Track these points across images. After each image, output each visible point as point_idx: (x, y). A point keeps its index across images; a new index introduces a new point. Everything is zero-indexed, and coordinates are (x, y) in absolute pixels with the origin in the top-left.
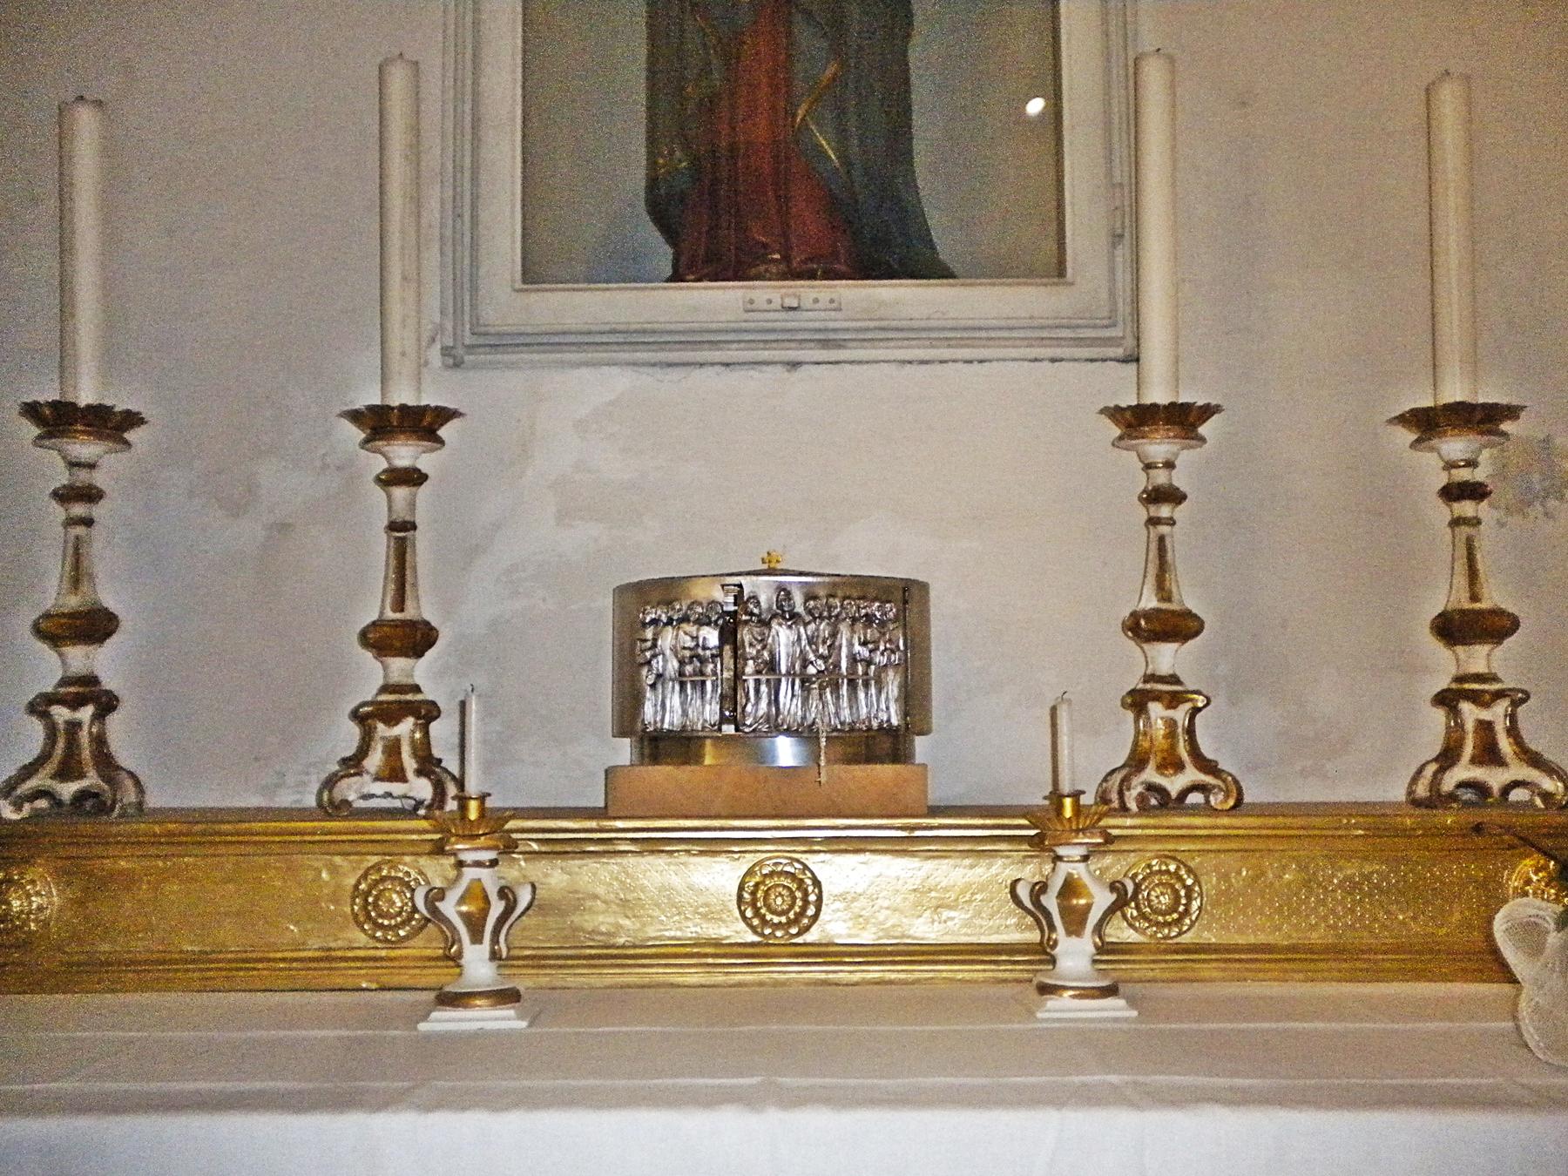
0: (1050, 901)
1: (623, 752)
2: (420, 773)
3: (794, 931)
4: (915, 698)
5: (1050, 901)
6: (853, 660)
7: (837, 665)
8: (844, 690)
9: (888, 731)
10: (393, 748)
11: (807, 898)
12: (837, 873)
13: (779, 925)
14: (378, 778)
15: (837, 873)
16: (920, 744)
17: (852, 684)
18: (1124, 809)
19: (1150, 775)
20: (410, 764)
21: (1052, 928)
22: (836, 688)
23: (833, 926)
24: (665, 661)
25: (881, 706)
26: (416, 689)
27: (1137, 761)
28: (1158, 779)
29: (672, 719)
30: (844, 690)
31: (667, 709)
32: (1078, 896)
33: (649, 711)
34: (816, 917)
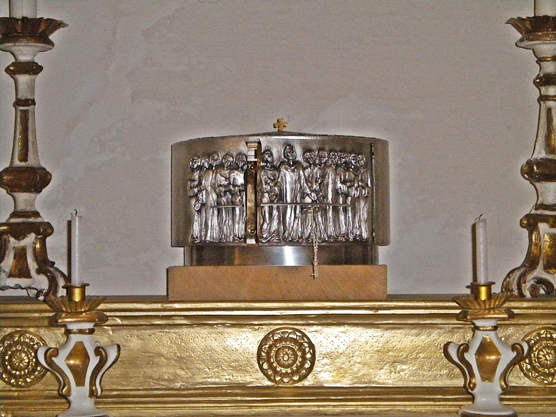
0: (471, 357)
1: (179, 256)
2: (39, 272)
3: (296, 378)
4: (378, 219)
5: (471, 357)
6: (336, 193)
7: (325, 197)
8: (330, 214)
9: (359, 241)
10: (21, 254)
11: (306, 354)
12: (325, 338)
13: (286, 375)
14: (11, 275)
15: (325, 338)
16: (382, 252)
17: (336, 210)
18: (521, 297)
19: (539, 272)
20: (32, 265)
21: (472, 375)
22: (325, 212)
23: (324, 375)
24: (208, 194)
25: (355, 224)
26: (36, 214)
27: (531, 262)
28: (546, 276)
29: (212, 235)
30: (330, 214)
31: (210, 226)
32: (491, 353)
33: (196, 228)
34: (310, 369)
